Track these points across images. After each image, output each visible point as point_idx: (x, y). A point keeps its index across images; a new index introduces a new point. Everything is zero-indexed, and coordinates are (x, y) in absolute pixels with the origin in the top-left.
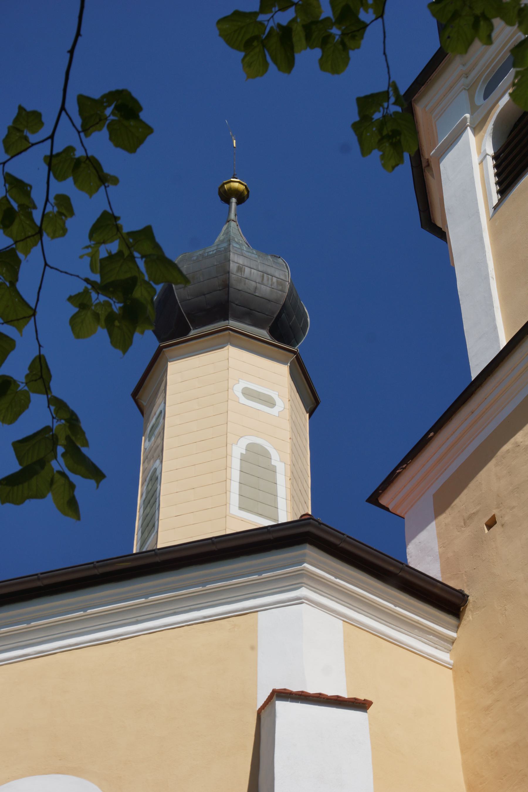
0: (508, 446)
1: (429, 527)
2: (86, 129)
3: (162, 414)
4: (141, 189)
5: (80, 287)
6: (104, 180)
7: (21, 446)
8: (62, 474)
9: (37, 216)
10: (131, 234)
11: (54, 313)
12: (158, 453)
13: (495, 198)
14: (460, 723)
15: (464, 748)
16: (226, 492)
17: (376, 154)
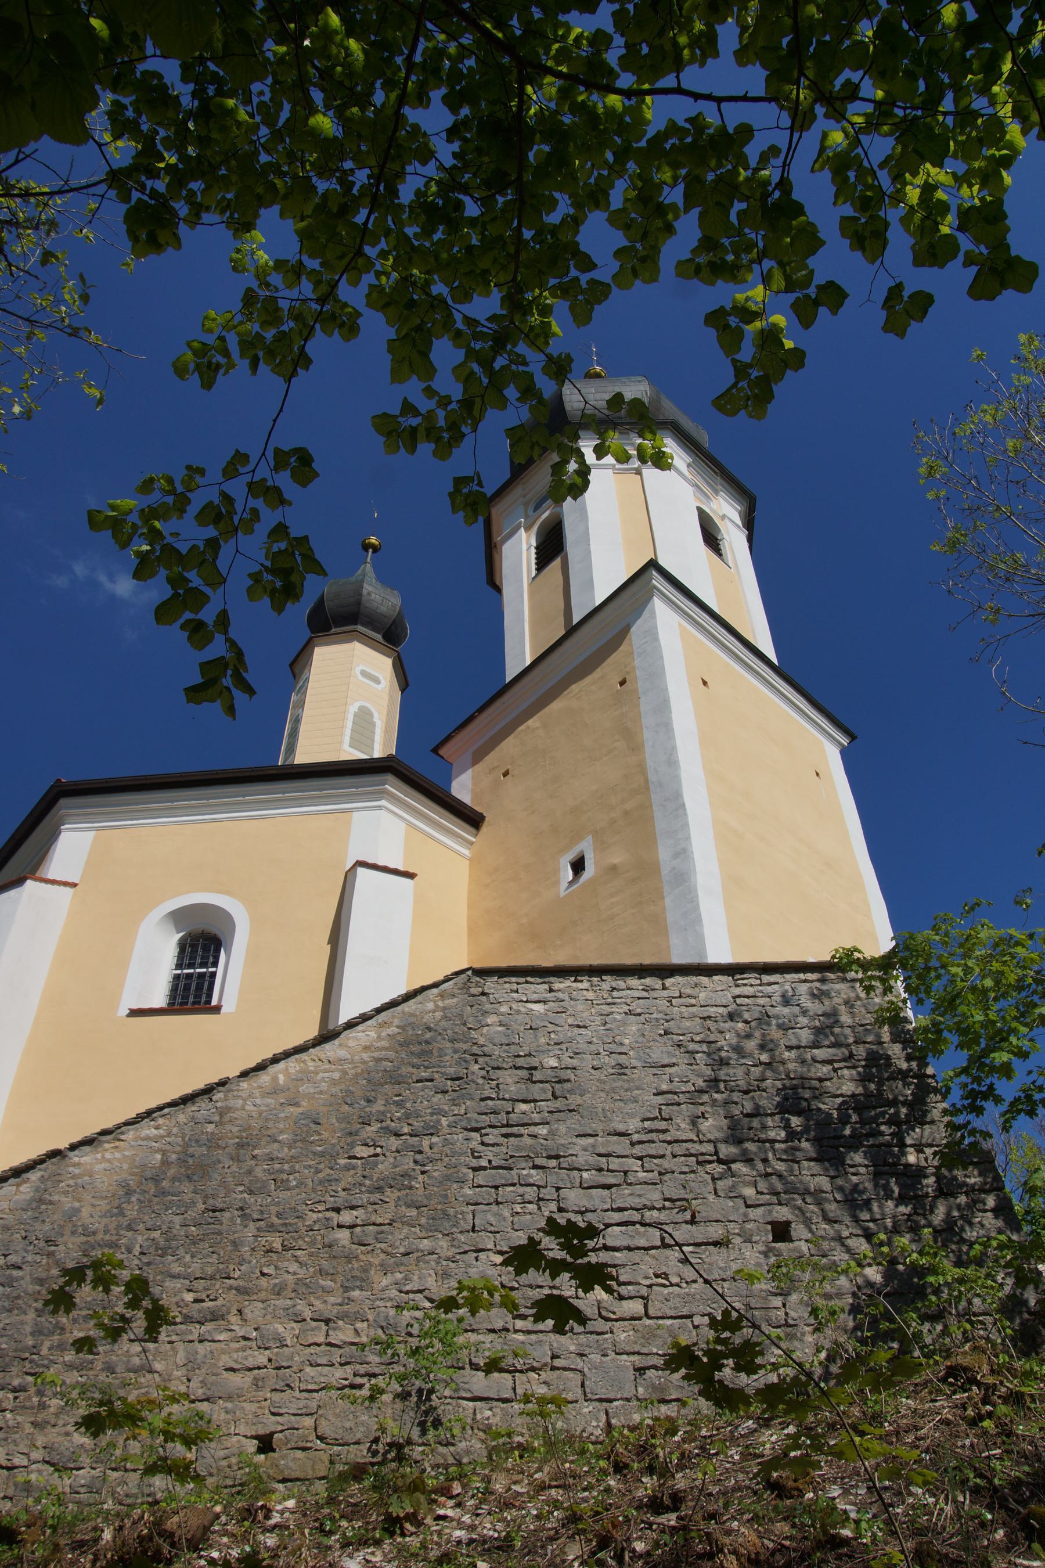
0: (522, 727)
2: (276, 469)
3: (307, 679)
4: (306, 512)
5: (257, 568)
6: (283, 502)
7: (204, 666)
8: (228, 689)
9: (236, 519)
10: (296, 539)
11: (238, 583)
12: (301, 704)
13: (534, 573)
15: (469, 907)
16: (342, 734)
17: (461, 514)
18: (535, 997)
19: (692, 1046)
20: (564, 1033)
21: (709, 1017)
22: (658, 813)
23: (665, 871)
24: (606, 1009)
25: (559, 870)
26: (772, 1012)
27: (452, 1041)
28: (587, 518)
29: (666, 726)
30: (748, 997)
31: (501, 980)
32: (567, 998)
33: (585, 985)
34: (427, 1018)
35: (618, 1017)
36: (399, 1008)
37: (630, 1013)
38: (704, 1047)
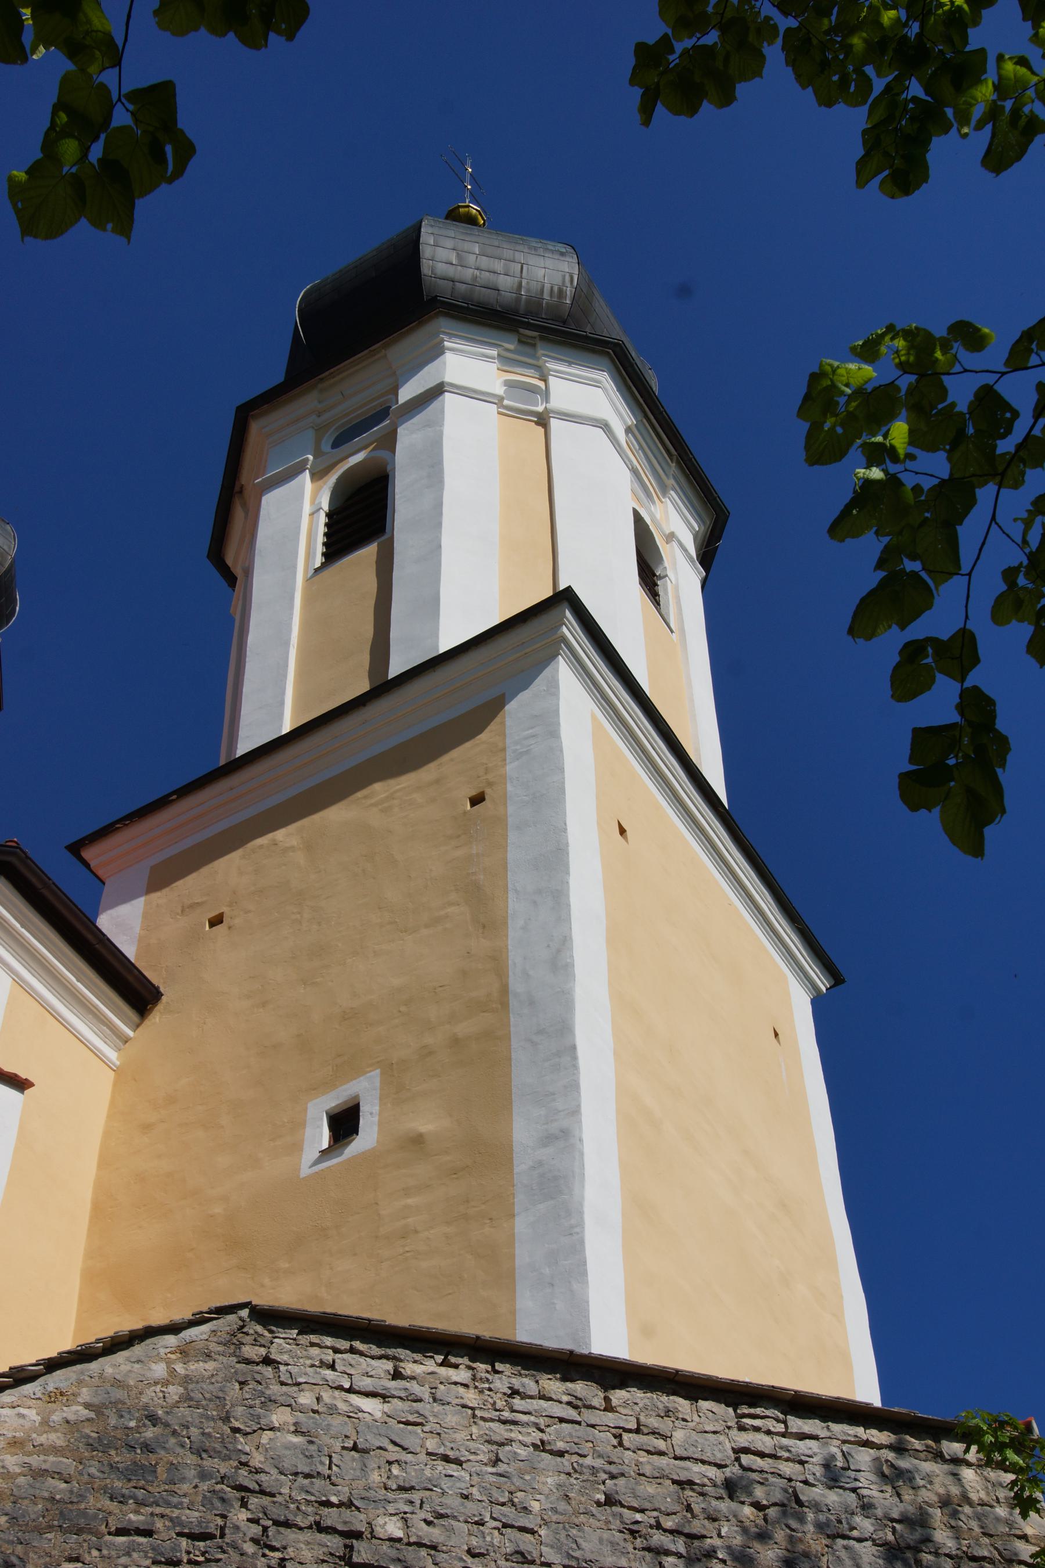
0: (259, 841)
1: (135, 902)
14: (107, 1134)
18: (366, 1384)
19: (658, 1538)
20: (419, 1469)
21: (690, 1483)
22: (519, 1054)
23: (521, 1166)
24: (501, 1432)
25: (303, 1125)
26: (807, 1494)
27: (199, 1451)
28: (441, 482)
29: (557, 898)
30: (762, 1455)
31: (304, 1339)
32: (426, 1396)
33: (462, 1375)
34: (150, 1396)
35: (522, 1452)
36: (94, 1366)
37: (541, 1447)
38: (680, 1545)
